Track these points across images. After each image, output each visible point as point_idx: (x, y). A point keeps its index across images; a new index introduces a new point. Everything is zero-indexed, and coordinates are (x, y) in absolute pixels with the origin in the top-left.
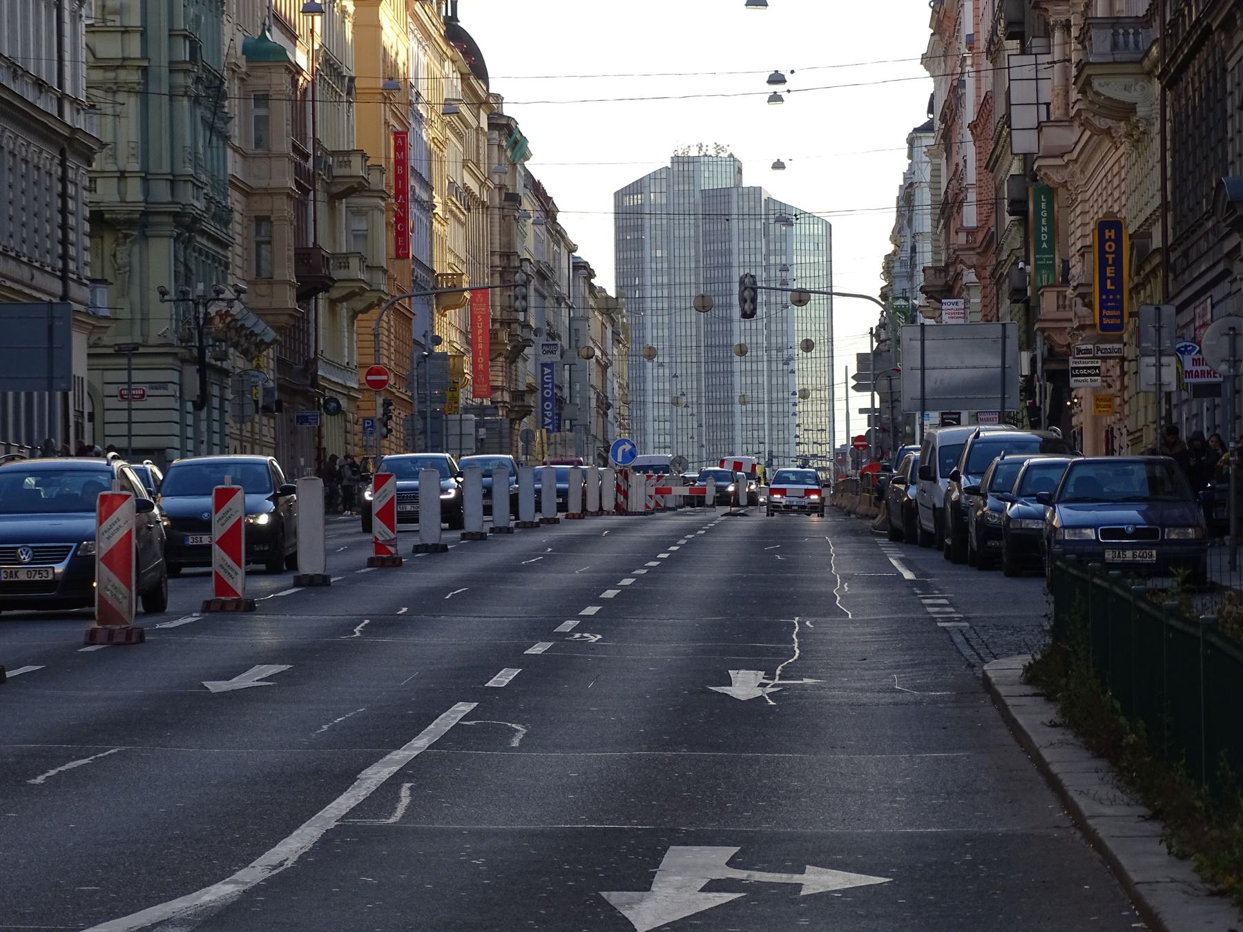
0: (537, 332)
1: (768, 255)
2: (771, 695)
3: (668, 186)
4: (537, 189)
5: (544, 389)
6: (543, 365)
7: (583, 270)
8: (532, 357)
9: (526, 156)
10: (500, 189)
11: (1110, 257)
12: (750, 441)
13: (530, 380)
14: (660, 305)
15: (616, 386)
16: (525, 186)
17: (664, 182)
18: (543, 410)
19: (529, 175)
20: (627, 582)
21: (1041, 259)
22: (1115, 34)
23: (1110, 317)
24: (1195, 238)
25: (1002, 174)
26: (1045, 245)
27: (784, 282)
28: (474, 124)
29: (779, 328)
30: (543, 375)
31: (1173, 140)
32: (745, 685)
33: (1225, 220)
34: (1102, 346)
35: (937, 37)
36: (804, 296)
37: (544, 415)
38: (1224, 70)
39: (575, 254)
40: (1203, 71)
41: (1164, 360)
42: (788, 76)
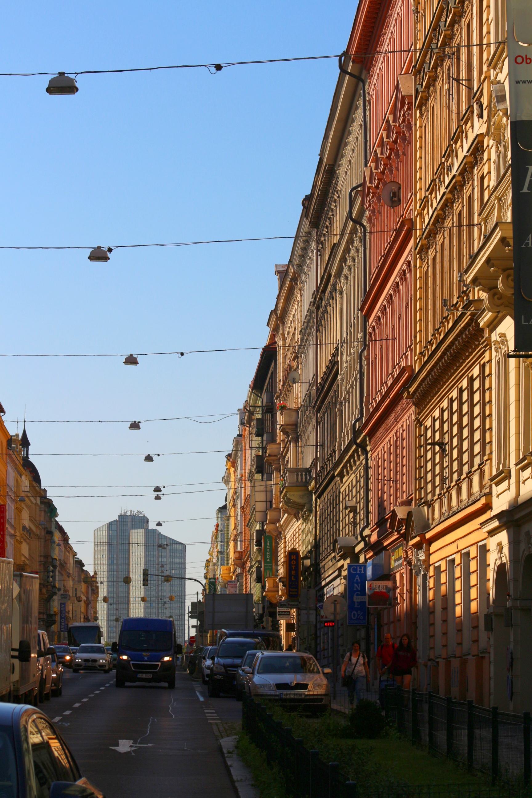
0: (59, 589)
1: (158, 558)
2: (134, 751)
4: (61, 529)
5: (61, 613)
6: (61, 604)
7: (80, 564)
8: (57, 600)
9: (56, 515)
10: (44, 529)
11: (293, 566)
13: (55, 609)
15: (92, 612)
16: (55, 528)
18: (61, 622)
19: (57, 523)
20: (85, 700)
21: (267, 566)
22: (297, 475)
23: (293, 592)
24: (327, 560)
25: (253, 529)
26: (268, 560)
27: (162, 572)
28: (34, 501)
30: (61, 608)
31: (320, 520)
32: (124, 746)
33: (338, 554)
34: (291, 603)
35: (486, 265)
36: (169, 578)
37: (61, 625)
38: (339, 492)
40: (332, 491)
41: (311, 612)
42: (162, 489)
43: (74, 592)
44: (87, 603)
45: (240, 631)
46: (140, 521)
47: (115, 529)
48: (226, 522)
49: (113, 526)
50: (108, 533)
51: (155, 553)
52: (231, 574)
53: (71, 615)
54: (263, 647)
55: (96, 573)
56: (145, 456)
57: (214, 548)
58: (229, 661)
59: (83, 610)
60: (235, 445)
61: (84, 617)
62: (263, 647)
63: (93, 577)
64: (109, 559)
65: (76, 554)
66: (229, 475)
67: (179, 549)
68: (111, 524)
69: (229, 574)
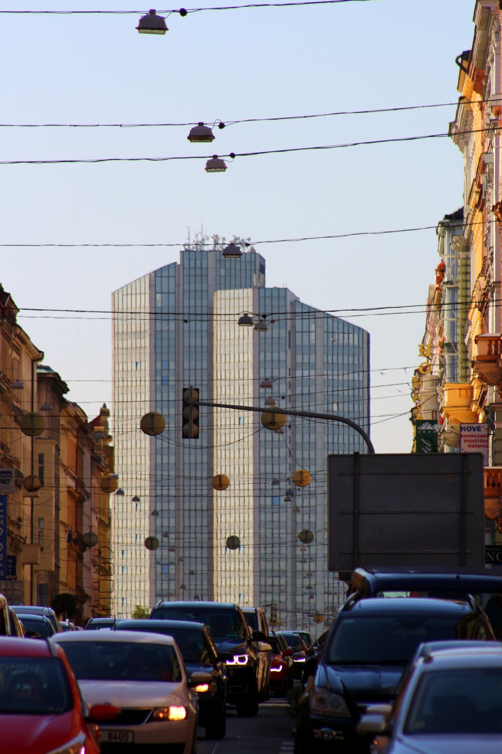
1: (294, 369)
3: (177, 286)
7: (55, 385)
12: (269, 589)
14: (165, 507)
15: (95, 523)
17: (172, 280)
29: (306, 455)
39: (44, 363)
42: (215, 131)
43: (37, 465)
44: (79, 497)
45: (413, 575)
46: (238, 262)
47: (172, 290)
48: (462, 254)
49: (165, 280)
50: (153, 301)
51: (283, 357)
52: (474, 407)
53: (25, 531)
54: (482, 630)
55: (104, 412)
56: (139, 17)
57: (434, 334)
58: (363, 677)
59: (64, 515)
60: (481, 22)
61: (70, 536)
62: (482, 630)
63: (97, 421)
64: (155, 373)
65: (40, 355)
66: (468, 115)
67: (351, 346)
68: (158, 276)
69: (469, 407)
